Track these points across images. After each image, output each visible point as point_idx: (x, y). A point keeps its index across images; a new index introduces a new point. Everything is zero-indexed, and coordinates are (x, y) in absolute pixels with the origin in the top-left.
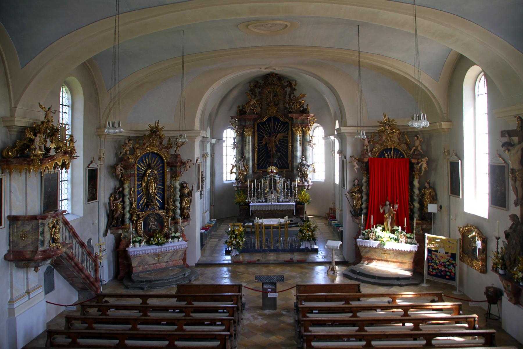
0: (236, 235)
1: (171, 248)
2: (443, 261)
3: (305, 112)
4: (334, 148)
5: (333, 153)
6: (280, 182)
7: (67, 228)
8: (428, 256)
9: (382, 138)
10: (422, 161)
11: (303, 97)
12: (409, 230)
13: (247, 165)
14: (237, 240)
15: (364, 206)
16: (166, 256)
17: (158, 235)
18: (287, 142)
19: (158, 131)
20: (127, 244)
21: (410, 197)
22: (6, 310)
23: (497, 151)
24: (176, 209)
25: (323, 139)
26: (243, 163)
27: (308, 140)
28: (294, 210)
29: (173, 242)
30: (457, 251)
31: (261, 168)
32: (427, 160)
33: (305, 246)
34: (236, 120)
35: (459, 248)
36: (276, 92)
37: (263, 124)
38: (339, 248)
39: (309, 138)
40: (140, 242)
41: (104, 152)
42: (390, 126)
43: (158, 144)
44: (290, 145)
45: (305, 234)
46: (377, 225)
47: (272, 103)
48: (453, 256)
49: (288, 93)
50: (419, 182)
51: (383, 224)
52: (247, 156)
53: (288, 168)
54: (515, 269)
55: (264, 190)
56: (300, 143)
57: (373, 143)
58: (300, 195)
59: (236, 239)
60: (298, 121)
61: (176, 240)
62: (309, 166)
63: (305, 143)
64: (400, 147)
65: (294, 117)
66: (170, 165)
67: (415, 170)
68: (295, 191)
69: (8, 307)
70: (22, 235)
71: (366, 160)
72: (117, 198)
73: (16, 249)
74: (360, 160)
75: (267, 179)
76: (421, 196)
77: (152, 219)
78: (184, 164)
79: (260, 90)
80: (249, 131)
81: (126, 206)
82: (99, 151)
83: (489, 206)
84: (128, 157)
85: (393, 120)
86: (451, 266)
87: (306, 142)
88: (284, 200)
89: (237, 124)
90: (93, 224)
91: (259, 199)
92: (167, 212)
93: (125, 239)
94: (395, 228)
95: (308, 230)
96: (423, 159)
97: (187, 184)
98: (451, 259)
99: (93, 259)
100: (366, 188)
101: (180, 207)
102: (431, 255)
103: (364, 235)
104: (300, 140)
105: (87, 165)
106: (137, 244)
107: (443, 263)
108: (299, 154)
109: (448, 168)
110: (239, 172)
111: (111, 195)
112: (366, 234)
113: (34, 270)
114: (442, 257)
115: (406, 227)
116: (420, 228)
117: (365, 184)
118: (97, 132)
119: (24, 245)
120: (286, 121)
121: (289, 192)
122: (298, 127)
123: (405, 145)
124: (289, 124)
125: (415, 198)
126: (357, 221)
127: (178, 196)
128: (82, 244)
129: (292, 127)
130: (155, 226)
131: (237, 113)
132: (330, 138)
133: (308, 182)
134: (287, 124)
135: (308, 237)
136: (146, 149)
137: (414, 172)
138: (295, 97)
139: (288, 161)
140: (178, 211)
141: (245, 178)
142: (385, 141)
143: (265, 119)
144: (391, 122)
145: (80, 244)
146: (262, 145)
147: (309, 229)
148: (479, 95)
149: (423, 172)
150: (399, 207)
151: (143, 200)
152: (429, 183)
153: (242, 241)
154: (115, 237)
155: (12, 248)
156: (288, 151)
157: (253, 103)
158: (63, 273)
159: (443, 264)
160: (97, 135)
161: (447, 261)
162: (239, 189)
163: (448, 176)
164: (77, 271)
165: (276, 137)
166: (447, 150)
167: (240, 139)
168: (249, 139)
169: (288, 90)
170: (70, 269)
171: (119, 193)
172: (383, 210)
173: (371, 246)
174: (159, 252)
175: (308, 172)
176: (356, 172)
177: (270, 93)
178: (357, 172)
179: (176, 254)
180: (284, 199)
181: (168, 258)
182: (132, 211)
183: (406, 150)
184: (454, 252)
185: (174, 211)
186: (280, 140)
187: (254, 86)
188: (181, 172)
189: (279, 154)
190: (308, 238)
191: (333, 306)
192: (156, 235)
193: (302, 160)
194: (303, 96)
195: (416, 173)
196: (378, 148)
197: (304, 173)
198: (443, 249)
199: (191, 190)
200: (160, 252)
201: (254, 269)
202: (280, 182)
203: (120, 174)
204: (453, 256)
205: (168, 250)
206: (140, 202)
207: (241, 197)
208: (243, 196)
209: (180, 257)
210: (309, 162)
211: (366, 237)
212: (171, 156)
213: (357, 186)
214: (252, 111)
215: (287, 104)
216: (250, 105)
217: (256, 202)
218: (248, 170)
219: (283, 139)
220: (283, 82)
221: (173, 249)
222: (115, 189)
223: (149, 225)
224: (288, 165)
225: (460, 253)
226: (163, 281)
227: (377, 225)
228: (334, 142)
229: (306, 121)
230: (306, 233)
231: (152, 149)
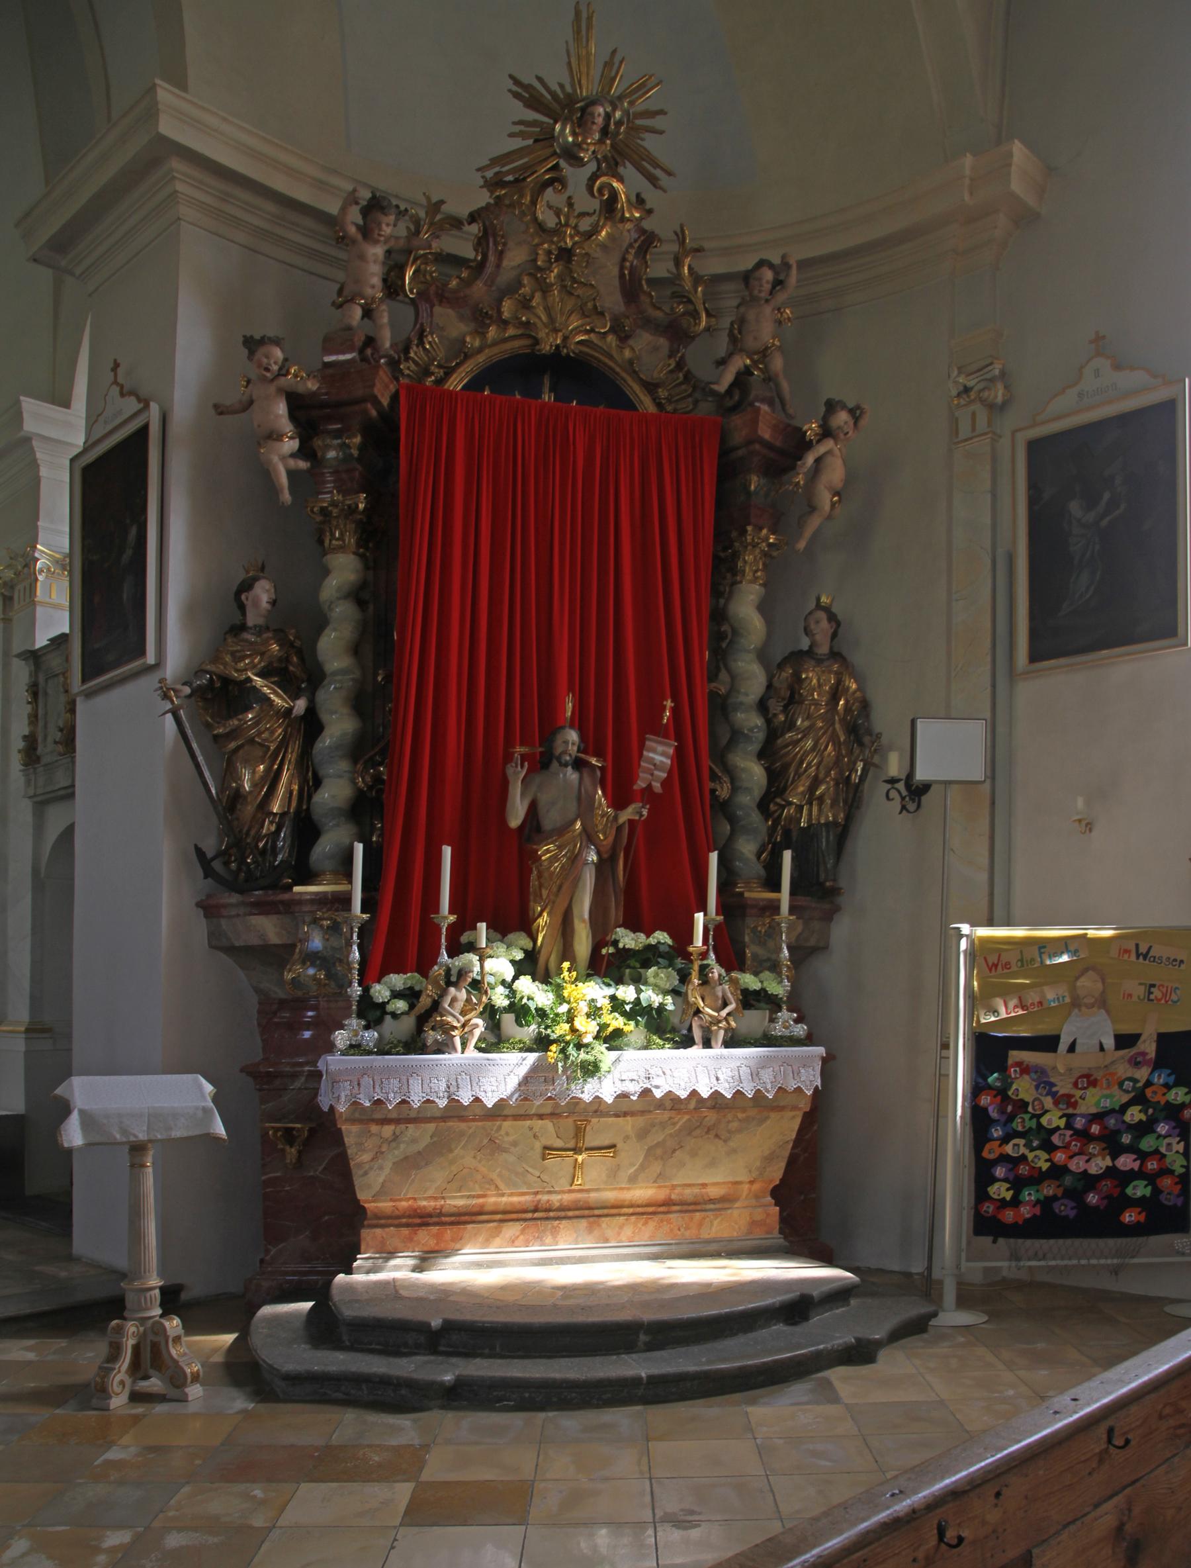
2: (1093, 1110)
8: (977, 1089)
50: (763, 607)
51: (526, 926)
64: (627, 353)
86: (1162, 1128)
102: (1007, 1083)
107: (1098, 1117)
114: (1091, 1081)
150: (679, 756)
161: (1125, 1098)
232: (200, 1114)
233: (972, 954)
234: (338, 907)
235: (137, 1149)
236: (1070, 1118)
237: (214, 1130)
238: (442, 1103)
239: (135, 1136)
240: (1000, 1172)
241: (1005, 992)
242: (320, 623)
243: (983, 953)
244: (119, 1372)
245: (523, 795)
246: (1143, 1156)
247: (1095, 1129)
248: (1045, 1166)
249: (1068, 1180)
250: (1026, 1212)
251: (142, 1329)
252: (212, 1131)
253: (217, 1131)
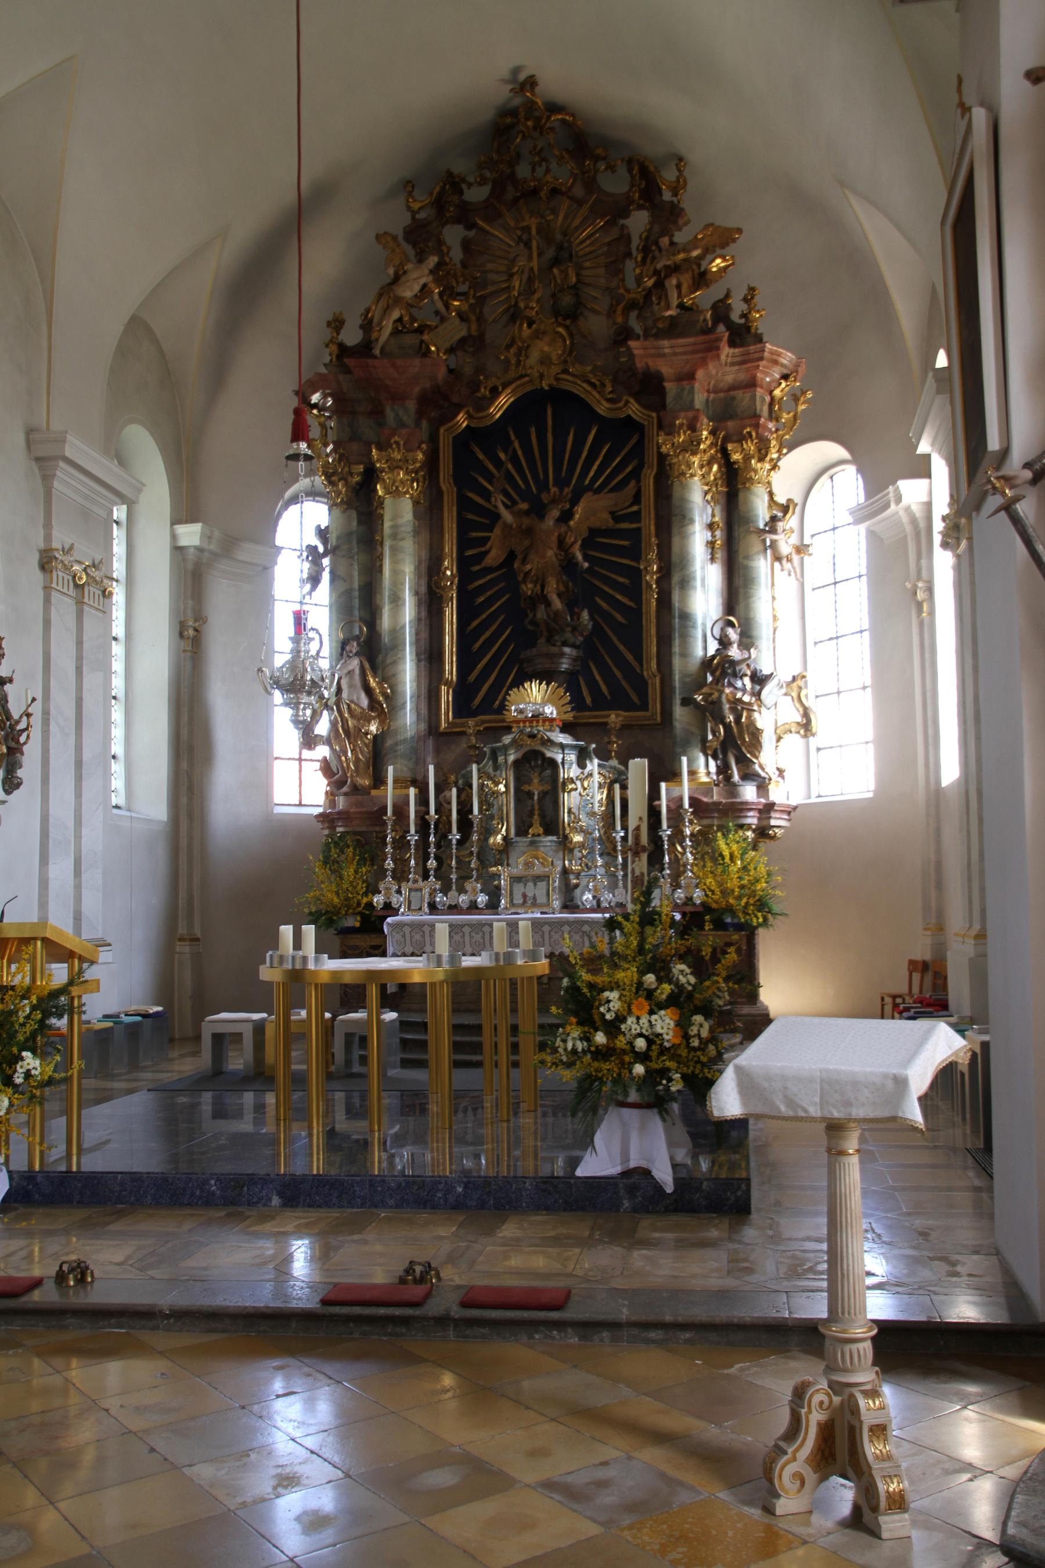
4: (924, 562)
5: (920, 595)
13: (389, 678)
18: (636, 552)
33: (625, 1157)
38: (915, 1114)
39: (762, 512)
44: (653, 555)
45: (613, 1028)
53: (644, 707)
55: (488, 831)
56: (711, 544)
58: (709, 864)
60: (692, 391)
62: (760, 680)
65: (666, 370)
75: (501, 759)
80: (394, 467)
87: (749, 532)
89: (331, 435)
91: (453, 893)
122: (693, 427)
132: (899, 499)
133: (763, 787)
135: (643, 1057)
139: (641, 665)
146: (489, 570)
147: (650, 978)
156: (638, 600)
157: (417, 288)
165: (566, 516)
169: (638, 221)
175: (764, 720)
177: (528, 245)
180: (445, 890)
186: (592, 539)
189: (585, 615)
190: (639, 1069)
193: (724, 643)
214: (410, 340)
224: (641, 685)
228: (922, 524)
230: (620, 1019)
232: (890, 1085)
235: (835, 1128)
237: (903, 1112)
239: (806, 1111)
244: (794, 1459)
251: (837, 1400)
252: (900, 1114)
253: (909, 1116)
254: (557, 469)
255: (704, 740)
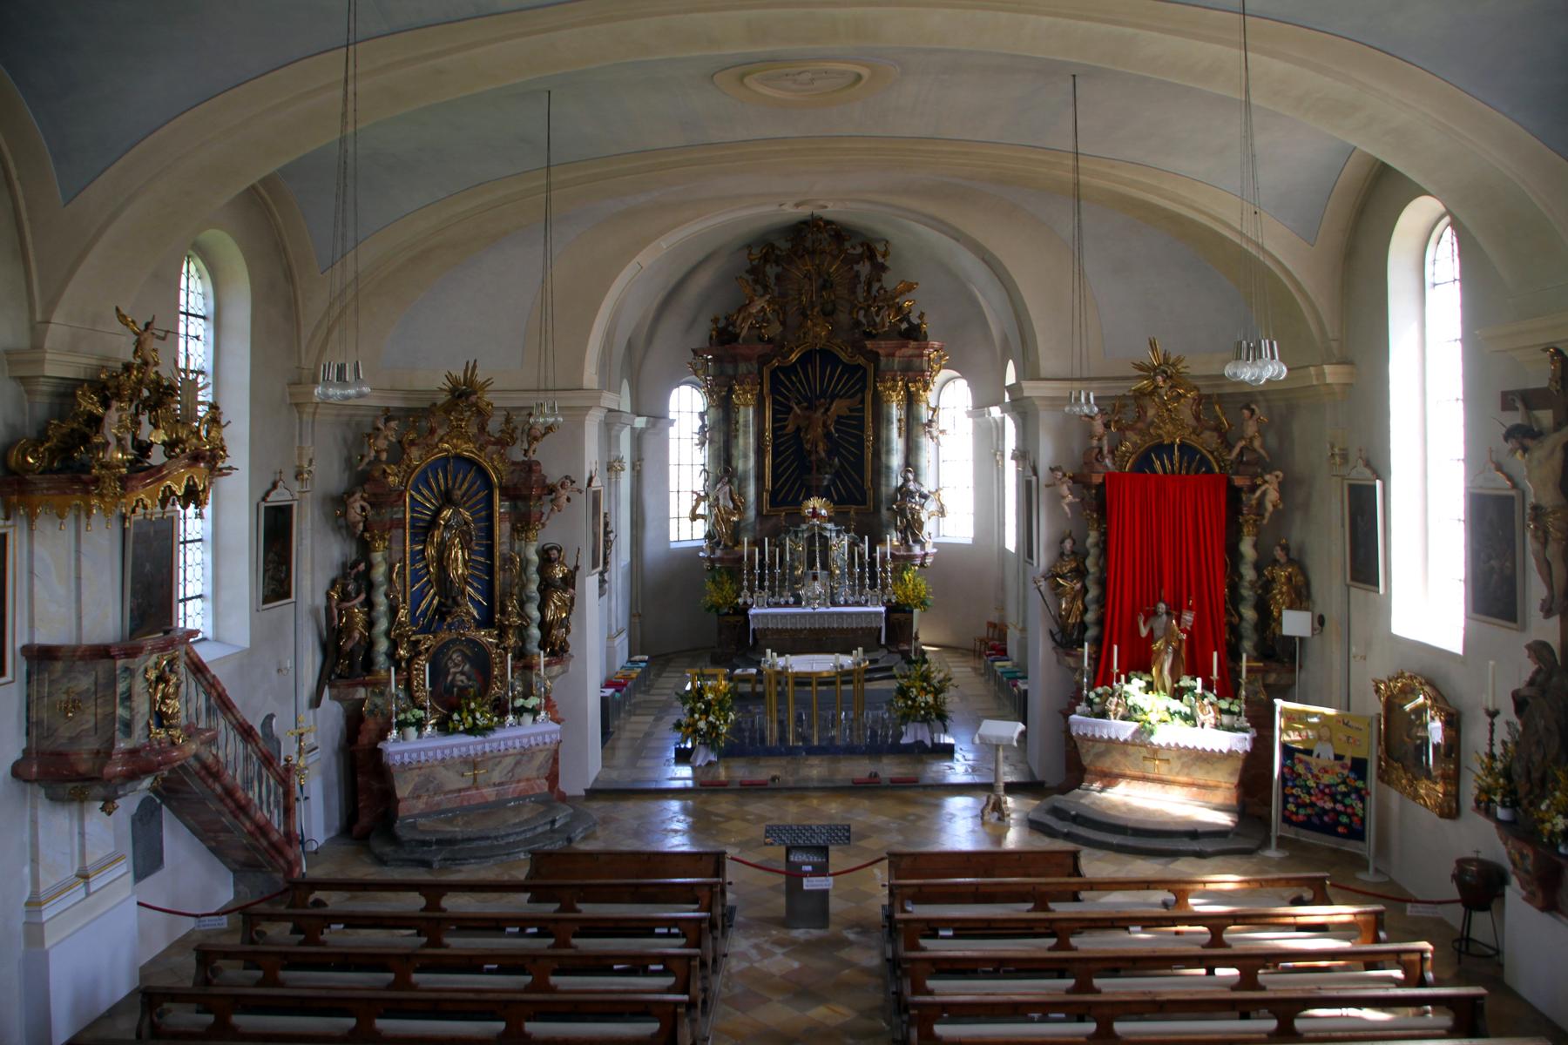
0: (708, 704)
1: (514, 743)
2: (1327, 783)
3: (914, 334)
4: (1000, 443)
5: (998, 458)
6: (840, 544)
7: (201, 684)
8: (1283, 766)
9: (1146, 413)
10: (1265, 482)
11: (909, 291)
12: (1227, 688)
13: (742, 494)
14: (711, 718)
15: (1090, 617)
16: (497, 765)
17: (473, 705)
18: (861, 427)
19: (475, 393)
20: (381, 730)
21: (1230, 591)
22: (19, 927)
23: (1491, 451)
24: (528, 625)
25: (969, 417)
26: (728, 488)
27: (925, 421)
28: (881, 628)
29: (519, 724)
30: (1371, 752)
31: (783, 502)
32: (1280, 479)
33: (916, 737)
34: (707, 360)
35: (1375, 742)
36: (826, 277)
37: (790, 370)
38: (1015, 744)
39: (925, 415)
40: (420, 725)
41: (311, 456)
42: (1170, 377)
43: (473, 430)
44: (870, 433)
45: (914, 700)
46: (1131, 674)
47: (816, 310)
48: (1359, 766)
49: (863, 279)
50: (1255, 546)
51: (1148, 671)
52: (741, 467)
53: (864, 503)
54: (1543, 807)
55: (793, 568)
56: (900, 429)
57: (1118, 429)
58: (899, 584)
59: (708, 717)
60: (893, 362)
61: (527, 718)
62: (925, 497)
63: (913, 428)
64: (1200, 441)
65: (881, 351)
66: (509, 493)
67: (1245, 510)
68: (885, 571)
69: (24, 920)
70: (67, 702)
71: (1097, 479)
72: (350, 593)
73: (47, 745)
74: (1078, 480)
75: (800, 535)
76: (1261, 587)
77: (454, 656)
78: (551, 490)
79: (779, 269)
80: (745, 392)
81: (378, 618)
82: (296, 452)
83: (1467, 617)
84: (385, 471)
85: (1179, 360)
86: (1353, 796)
87: (918, 424)
88: (851, 599)
89: (711, 371)
90: (279, 670)
91: (777, 597)
92: (502, 636)
93: (376, 716)
94: (1185, 682)
95: (923, 689)
96: (1267, 477)
97: (559, 551)
98: (1352, 776)
99: (278, 774)
100: (1097, 564)
101: (538, 620)
102: (1294, 764)
103: (1090, 702)
104: (899, 420)
105: (261, 494)
106: (412, 732)
107: (1328, 786)
108: (896, 460)
109: (1342, 502)
110: (716, 516)
111: (333, 583)
112: (1097, 700)
113: (103, 809)
114: (1325, 771)
115: (1217, 681)
116: (1261, 682)
117: (1093, 551)
118: (291, 395)
119: (73, 735)
120: (856, 363)
121: (868, 574)
122: (894, 380)
123: (1215, 434)
124: (865, 370)
125: (1246, 592)
126: (1071, 661)
127: (533, 587)
128: (245, 731)
129: (875, 381)
130: (463, 678)
131: (711, 338)
132: (990, 414)
133: (923, 545)
134: (861, 371)
135: (923, 709)
136: (437, 447)
137: (1242, 514)
138: (886, 291)
139: (863, 482)
140: (535, 632)
141: (736, 532)
142: (1153, 422)
143: (794, 357)
144: (1174, 365)
145: (240, 729)
146: (787, 435)
147: (925, 684)
148: (1435, 285)
149: (1267, 515)
150: (1197, 619)
151: (428, 598)
152: (1286, 548)
153: (726, 721)
154: (346, 710)
155: (37, 743)
156: (863, 453)
157: (759, 308)
158: (188, 818)
159: (1327, 791)
160: (291, 404)
161: (1339, 781)
162: (718, 565)
163: (1343, 526)
164: (232, 812)
165: (827, 410)
166: (1340, 449)
167: (721, 415)
168: (747, 415)
169: (864, 269)
170: (211, 806)
171: (356, 579)
172: (1148, 628)
173: (1114, 737)
174: (476, 754)
175: (924, 516)
176: (1066, 514)
177: (810, 279)
178: (1069, 516)
179: (529, 761)
180: (853, 595)
181: (505, 772)
182: (395, 631)
183: (1217, 449)
184: (1360, 754)
185: (522, 631)
186: (839, 420)
187: (760, 258)
188: (541, 516)
189: (836, 460)
190: (923, 712)
191: (999, 917)
192: (468, 704)
193: (906, 480)
194: (910, 287)
195: (1248, 517)
196: (1134, 444)
197: (913, 517)
198: (1329, 746)
199: (572, 569)
200: (479, 753)
201: (760, 805)
202: (840, 544)
203: (359, 522)
204: (1359, 766)
205: (502, 747)
206: (419, 606)
207: (722, 590)
208: (727, 586)
209: (538, 769)
210: (928, 485)
211: (1096, 709)
212: (513, 468)
213: (1072, 557)
214: (755, 332)
215: (862, 313)
216: (750, 314)
217: (768, 604)
218: (745, 509)
219: (847, 418)
220: (847, 245)
221: (518, 745)
222: (344, 565)
223: (448, 673)
224: (863, 493)
225: (1380, 759)
226: (489, 842)
227: (1131, 674)
228: (1000, 425)
229: (916, 361)
230: (916, 697)
231: (455, 447)
233: (1281, 713)
234: (980, 669)
235: (997, 747)
236: (1317, 784)
238: (1106, 737)
240: (1291, 799)
241: (1294, 729)
242: (1086, 555)
243: (1284, 712)
245: (1145, 624)
246: (1345, 806)
247: (1327, 791)
248: (1308, 801)
249: (1317, 809)
250: (1301, 818)
254: (821, 385)
255: (896, 525)
